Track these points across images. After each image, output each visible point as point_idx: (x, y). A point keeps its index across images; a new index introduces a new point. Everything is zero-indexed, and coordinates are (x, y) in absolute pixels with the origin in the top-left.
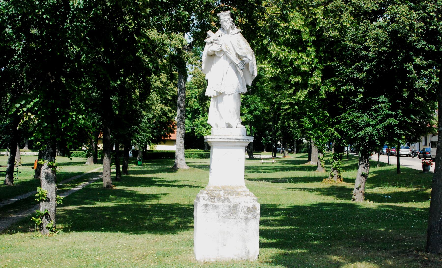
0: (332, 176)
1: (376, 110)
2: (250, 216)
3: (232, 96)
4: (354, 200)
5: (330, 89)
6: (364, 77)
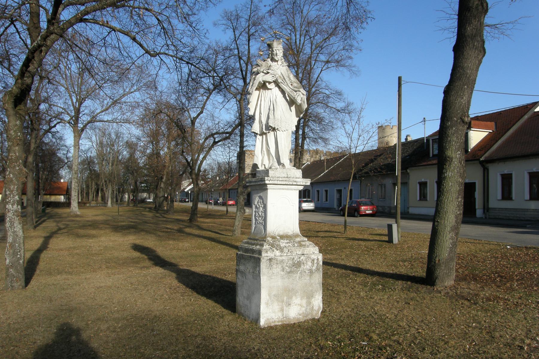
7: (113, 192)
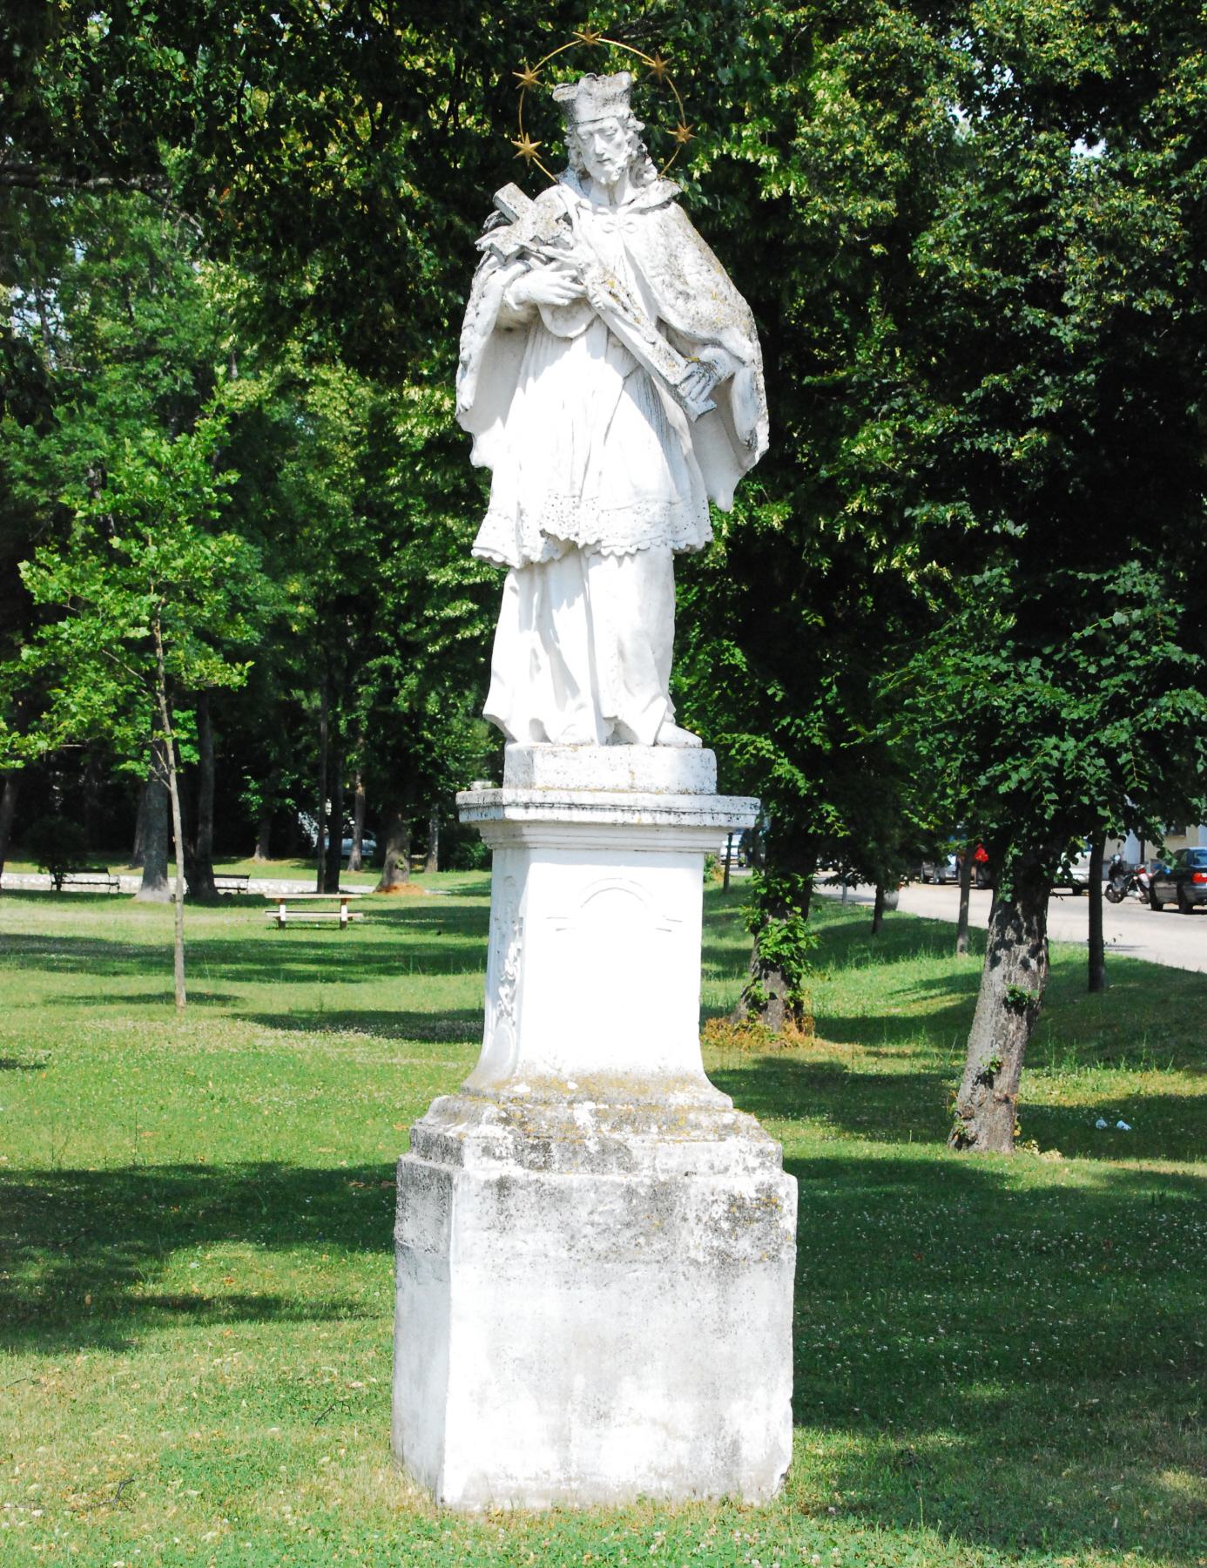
0: (757, 1005)
1: (1093, 647)
2: (744, 1246)
3: (633, 569)
4: (964, 1142)
5: (761, 513)
6: (1035, 453)
7: (168, 1200)
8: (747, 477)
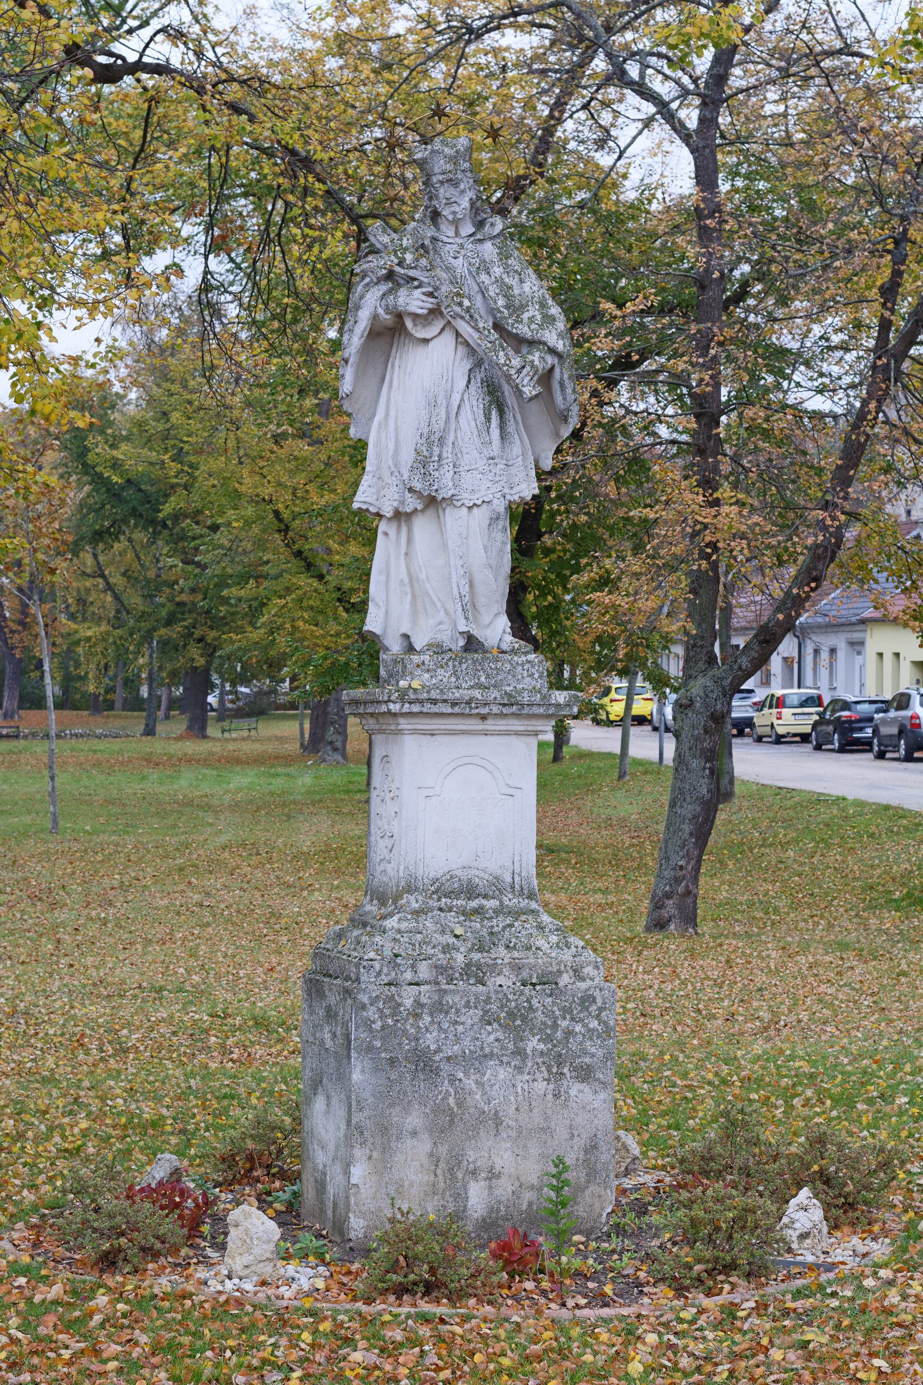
8: (368, 599)
